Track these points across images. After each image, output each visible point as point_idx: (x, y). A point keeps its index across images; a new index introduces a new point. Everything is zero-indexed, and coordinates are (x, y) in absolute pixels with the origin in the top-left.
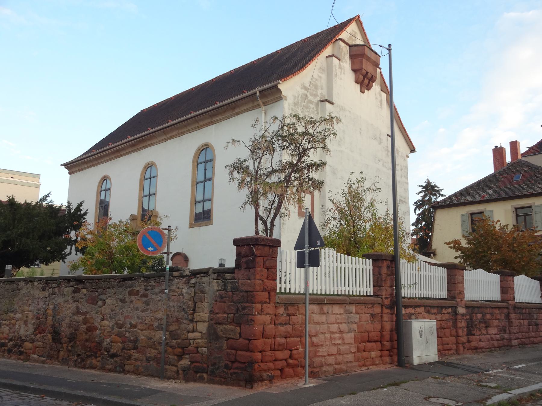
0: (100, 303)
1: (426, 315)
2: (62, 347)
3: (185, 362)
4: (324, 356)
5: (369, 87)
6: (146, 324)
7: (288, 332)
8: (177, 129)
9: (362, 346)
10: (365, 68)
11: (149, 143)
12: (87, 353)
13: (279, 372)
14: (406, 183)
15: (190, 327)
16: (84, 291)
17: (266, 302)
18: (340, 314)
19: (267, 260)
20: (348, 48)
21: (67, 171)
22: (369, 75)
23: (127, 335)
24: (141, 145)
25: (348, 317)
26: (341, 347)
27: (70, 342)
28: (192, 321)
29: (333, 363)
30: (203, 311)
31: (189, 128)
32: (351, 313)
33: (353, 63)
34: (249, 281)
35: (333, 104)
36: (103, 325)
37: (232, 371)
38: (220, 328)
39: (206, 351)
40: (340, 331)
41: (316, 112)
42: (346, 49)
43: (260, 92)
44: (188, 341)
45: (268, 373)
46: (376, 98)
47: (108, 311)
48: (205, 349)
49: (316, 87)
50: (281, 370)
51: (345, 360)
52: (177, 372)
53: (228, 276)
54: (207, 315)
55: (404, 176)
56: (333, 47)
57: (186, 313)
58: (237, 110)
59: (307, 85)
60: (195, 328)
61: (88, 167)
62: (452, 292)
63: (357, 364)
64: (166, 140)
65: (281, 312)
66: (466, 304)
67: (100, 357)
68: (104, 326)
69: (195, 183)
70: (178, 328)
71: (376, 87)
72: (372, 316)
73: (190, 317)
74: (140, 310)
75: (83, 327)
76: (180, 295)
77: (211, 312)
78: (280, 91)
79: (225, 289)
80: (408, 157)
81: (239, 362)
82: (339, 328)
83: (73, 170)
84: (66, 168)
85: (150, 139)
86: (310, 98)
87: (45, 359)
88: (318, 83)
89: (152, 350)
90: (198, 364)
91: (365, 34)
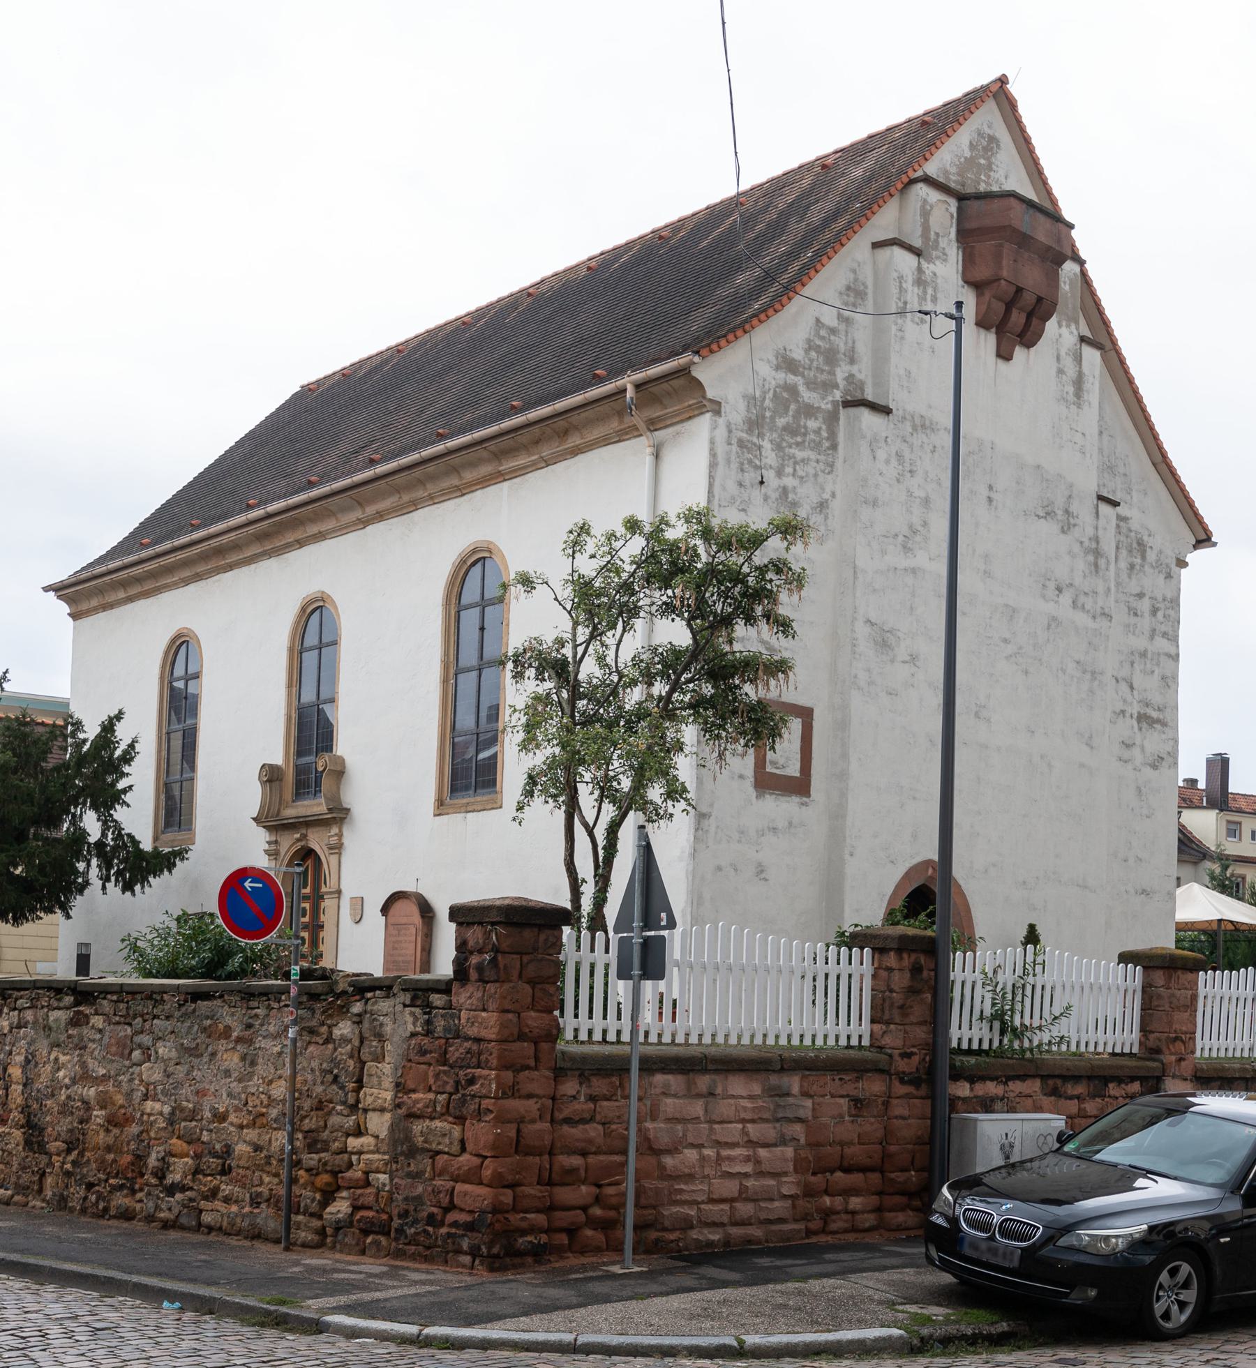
0: (137, 1054)
1: (1046, 1101)
2: (50, 1164)
3: (340, 1207)
4: (698, 1203)
5: (1028, 336)
6: (250, 1112)
7: (590, 1141)
8: (398, 490)
9: (817, 1180)
10: (1020, 269)
11: (313, 529)
12: (111, 1181)
13: (563, 1239)
14: (1169, 656)
15: (350, 1122)
16: (97, 1021)
17: (528, 1068)
18: (751, 1097)
19: (530, 962)
20: (953, 205)
21: (64, 608)
22: (1028, 299)
23: (205, 1137)
24: (290, 537)
25: (778, 1106)
26: (750, 1183)
27: (69, 1151)
28: (354, 1108)
29: (725, 1220)
30: (380, 1084)
31: (431, 488)
32: (788, 1095)
33: (969, 261)
34: (484, 1014)
35: (886, 411)
36: (148, 1110)
37: (444, 1230)
38: (418, 1127)
39: (387, 1181)
40: (750, 1141)
41: (826, 444)
42: (943, 212)
43: (638, 386)
44: (346, 1156)
45: (529, 1238)
46: (1060, 372)
47: (157, 1076)
48: (383, 1178)
49: (831, 357)
50: (572, 1231)
51: (763, 1216)
52: (322, 1232)
53: (437, 999)
54: (388, 1096)
55: (1165, 635)
56: (901, 208)
57: (342, 1088)
58: (574, 440)
59: (798, 354)
60: (362, 1127)
61: (130, 599)
62: (1152, 1036)
63: (800, 1226)
64: (364, 523)
65: (571, 1092)
66: (1196, 1070)
67: (141, 1190)
68: (149, 1115)
69: (453, 670)
70: (322, 1123)
71: (1059, 334)
72: (858, 1103)
73: (351, 1099)
74: (235, 1075)
75: (98, 1115)
76: (327, 1042)
77: (399, 1087)
78: (698, 385)
79: (428, 1033)
80: (1182, 564)
81: (462, 1210)
82: (744, 1132)
83: (84, 606)
84: (58, 597)
85: (316, 518)
86: (807, 396)
87: (9, 1192)
88: (840, 343)
89: (264, 1176)
90: (371, 1214)
91: (1027, 141)
